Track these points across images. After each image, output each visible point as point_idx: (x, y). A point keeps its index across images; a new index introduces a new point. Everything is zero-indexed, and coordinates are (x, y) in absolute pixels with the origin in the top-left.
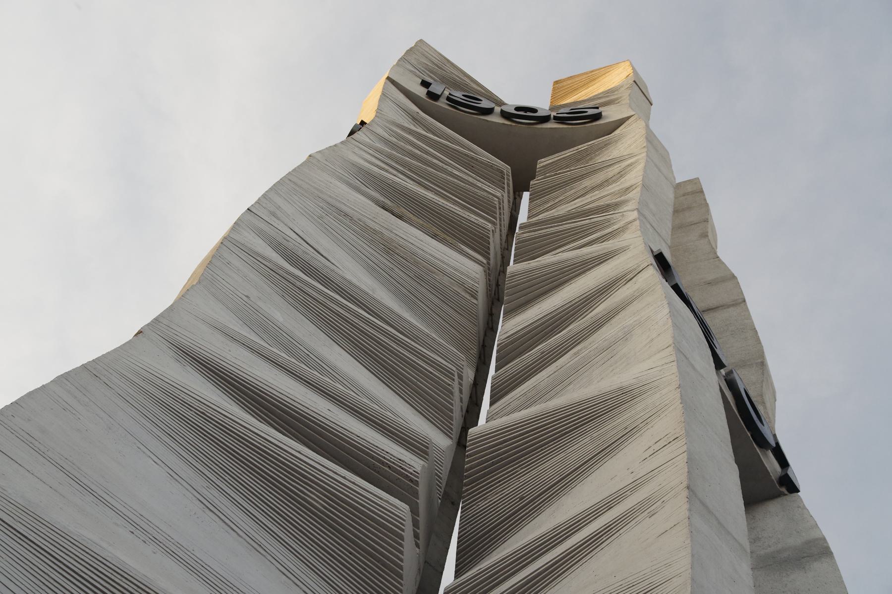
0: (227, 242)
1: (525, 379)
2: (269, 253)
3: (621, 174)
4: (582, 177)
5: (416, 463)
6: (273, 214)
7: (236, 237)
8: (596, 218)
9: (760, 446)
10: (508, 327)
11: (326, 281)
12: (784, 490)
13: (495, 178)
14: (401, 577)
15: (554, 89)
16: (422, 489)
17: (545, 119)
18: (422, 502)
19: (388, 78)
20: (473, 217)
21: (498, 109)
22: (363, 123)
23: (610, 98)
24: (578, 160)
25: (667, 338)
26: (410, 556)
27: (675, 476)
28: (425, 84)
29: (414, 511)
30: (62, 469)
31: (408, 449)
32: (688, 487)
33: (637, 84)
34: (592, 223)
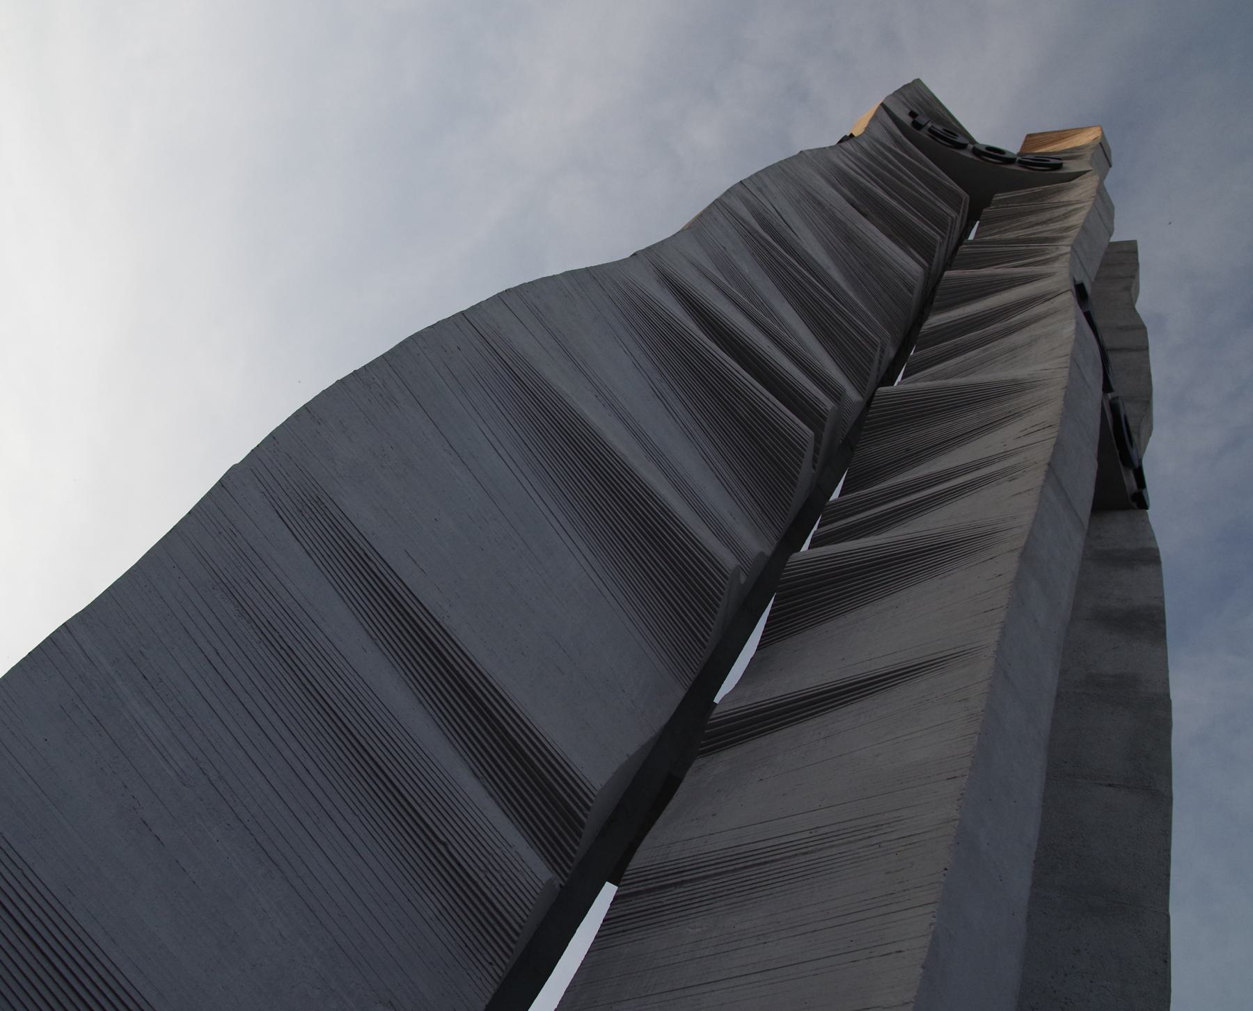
0: (719, 204)
1: (721, 746)
2: (749, 219)
3: (1066, 216)
4: (1032, 213)
5: (828, 404)
6: (760, 190)
7: (727, 201)
8: (1033, 246)
9: (1124, 464)
10: (935, 320)
11: (791, 250)
12: (1134, 504)
13: (954, 201)
14: (795, 485)
15: (1026, 141)
16: (828, 425)
17: (1011, 161)
18: (826, 435)
19: (882, 105)
20: (926, 228)
21: (970, 146)
22: (852, 135)
23: (1074, 154)
24: (1030, 200)
25: (1068, 349)
26: (806, 472)
27: (1041, 454)
28: (912, 114)
29: (818, 439)
30: (555, 338)
31: (824, 392)
32: (1049, 464)
33: (1102, 148)
34: (1032, 249)
